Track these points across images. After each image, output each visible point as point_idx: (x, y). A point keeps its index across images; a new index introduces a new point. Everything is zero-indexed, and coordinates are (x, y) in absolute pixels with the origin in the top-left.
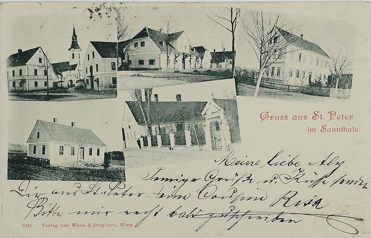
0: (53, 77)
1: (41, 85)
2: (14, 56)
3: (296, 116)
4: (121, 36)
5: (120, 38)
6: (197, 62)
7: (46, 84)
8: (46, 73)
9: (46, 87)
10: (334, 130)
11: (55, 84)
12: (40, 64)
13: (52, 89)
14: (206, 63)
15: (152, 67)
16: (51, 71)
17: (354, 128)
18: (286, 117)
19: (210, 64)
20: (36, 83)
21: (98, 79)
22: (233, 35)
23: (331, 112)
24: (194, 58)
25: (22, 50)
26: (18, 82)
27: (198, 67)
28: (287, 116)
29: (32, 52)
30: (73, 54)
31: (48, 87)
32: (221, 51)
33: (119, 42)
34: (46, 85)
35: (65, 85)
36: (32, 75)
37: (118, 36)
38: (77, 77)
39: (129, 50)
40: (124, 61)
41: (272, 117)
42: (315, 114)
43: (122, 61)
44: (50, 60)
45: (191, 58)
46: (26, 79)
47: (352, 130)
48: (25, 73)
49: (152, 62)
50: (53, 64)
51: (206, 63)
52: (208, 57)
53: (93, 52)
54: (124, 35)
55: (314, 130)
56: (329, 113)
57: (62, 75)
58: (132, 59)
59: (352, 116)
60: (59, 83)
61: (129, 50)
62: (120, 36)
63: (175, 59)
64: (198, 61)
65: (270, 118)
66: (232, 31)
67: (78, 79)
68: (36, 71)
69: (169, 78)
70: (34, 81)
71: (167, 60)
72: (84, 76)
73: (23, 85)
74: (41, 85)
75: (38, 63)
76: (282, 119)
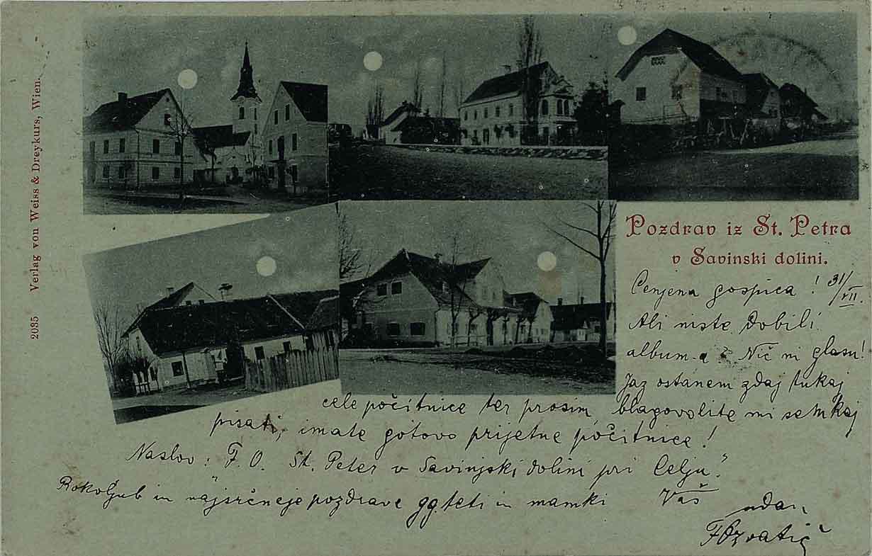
0: (196, 162)
1: (167, 174)
2: (106, 110)
4: (347, 271)
5: (345, 275)
6: (520, 328)
8: (179, 148)
12: (168, 129)
13: (189, 185)
14: (541, 328)
15: (418, 338)
16: (189, 146)
19: (550, 332)
20: (156, 172)
21: (295, 167)
22: (603, 267)
24: (513, 320)
25: (126, 95)
26: (116, 167)
27: (523, 339)
30: (242, 110)
31: (182, 180)
32: (575, 302)
33: (343, 283)
37: (340, 269)
38: (249, 162)
39: (366, 302)
40: (354, 327)
42: (760, 223)
43: (350, 327)
45: (507, 318)
46: (134, 161)
48: (131, 147)
49: (418, 328)
51: (541, 328)
52: (544, 319)
53: (288, 107)
54: (353, 267)
56: (792, 219)
57: (214, 156)
58: (372, 323)
60: (208, 173)
61: (366, 302)
62: (346, 270)
63: (471, 321)
64: (522, 326)
66: (599, 256)
67: (249, 166)
68: (156, 143)
69: (457, 365)
70: (150, 166)
71: (453, 325)
73: (126, 174)
74: (167, 174)
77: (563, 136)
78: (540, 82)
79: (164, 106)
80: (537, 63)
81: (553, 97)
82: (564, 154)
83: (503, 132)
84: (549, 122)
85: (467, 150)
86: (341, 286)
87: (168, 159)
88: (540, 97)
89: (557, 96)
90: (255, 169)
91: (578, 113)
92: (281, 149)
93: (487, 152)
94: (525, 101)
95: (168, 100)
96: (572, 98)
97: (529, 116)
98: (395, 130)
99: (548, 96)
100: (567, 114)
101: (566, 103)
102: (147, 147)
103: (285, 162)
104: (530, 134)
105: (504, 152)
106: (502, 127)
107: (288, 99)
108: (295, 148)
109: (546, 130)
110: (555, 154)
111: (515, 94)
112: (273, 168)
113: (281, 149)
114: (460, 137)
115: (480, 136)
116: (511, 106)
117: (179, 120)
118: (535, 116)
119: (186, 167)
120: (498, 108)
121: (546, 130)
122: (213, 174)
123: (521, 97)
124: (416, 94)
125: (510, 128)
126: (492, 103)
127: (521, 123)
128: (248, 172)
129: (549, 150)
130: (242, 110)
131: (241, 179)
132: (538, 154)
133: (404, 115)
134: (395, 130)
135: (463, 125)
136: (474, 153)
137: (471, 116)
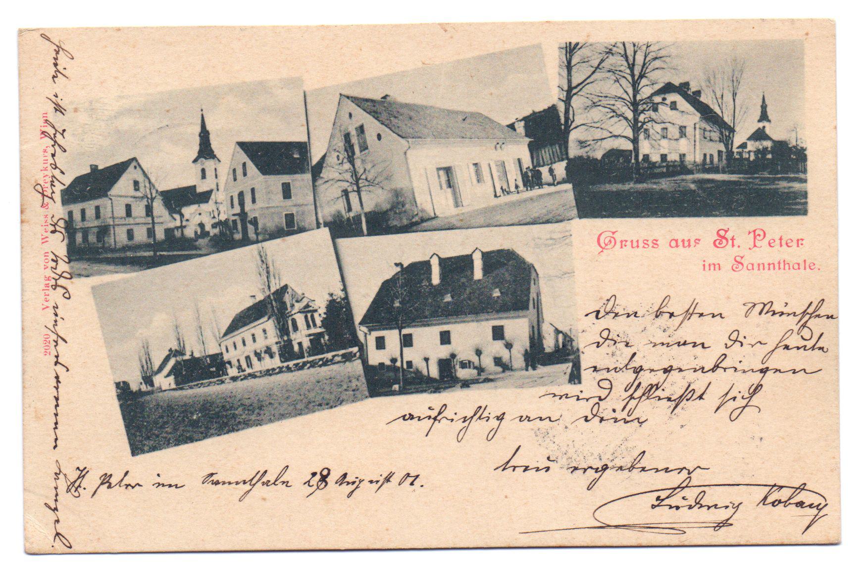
0: (164, 219)
1: (141, 235)
3: (677, 241)
7: (151, 233)
8: (149, 210)
9: (151, 241)
10: (761, 267)
11: (169, 232)
13: (163, 242)
16: (159, 207)
17: (807, 262)
18: (655, 243)
20: (130, 234)
21: (255, 218)
23: (754, 231)
28: (657, 241)
29: (117, 171)
30: (203, 171)
34: (149, 236)
35: (189, 232)
36: (119, 216)
41: (624, 243)
44: (156, 185)
46: (110, 225)
47: (802, 266)
48: (106, 212)
50: (162, 192)
53: (244, 164)
55: (717, 266)
57: (182, 215)
59: (802, 240)
65: (618, 244)
67: (216, 220)
68: (128, 208)
70: (125, 229)
72: (226, 213)
74: (141, 235)
75: (132, 192)
76: (646, 246)
77: (316, 346)
78: (284, 303)
79: (130, 175)
80: (278, 287)
81: (299, 314)
82: (321, 363)
83: (263, 355)
84: (301, 337)
85: (234, 379)
86: (527, 135)
87: (142, 220)
88: (288, 317)
89: (303, 312)
90: (220, 223)
91: (324, 323)
92: (242, 204)
93: (253, 376)
94: (276, 324)
95: (135, 167)
96: (316, 311)
97: (282, 336)
98: (168, 375)
99: (295, 314)
100: (315, 325)
101: (312, 316)
102: (121, 211)
103: (246, 214)
104: (287, 352)
105: (269, 373)
106: (261, 351)
107: (243, 157)
108: (254, 201)
109: (300, 344)
110: (313, 364)
111: (266, 318)
112: (235, 220)
113: (242, 204)
114: (226, 369)
115: (244, 365)
116: (264, 331)
117: (148, 185)
118: (288, 334)
119: (157, 228)
120: (253, 335)
121: (300, 344)
122: (182, 231)
123: (271, 321)
124: (179, 339)
125: (269, 351)
126: (245, 333)
127: (277, 343)
128: (214, 226)
129: (308, 362)
130: (203, 171)
131: (208, 233)
132: (300, 368)
133: (172, 362)
134: (168, 375)
135: (226, 357)
136: (242, 380)
137: (231, 348)
